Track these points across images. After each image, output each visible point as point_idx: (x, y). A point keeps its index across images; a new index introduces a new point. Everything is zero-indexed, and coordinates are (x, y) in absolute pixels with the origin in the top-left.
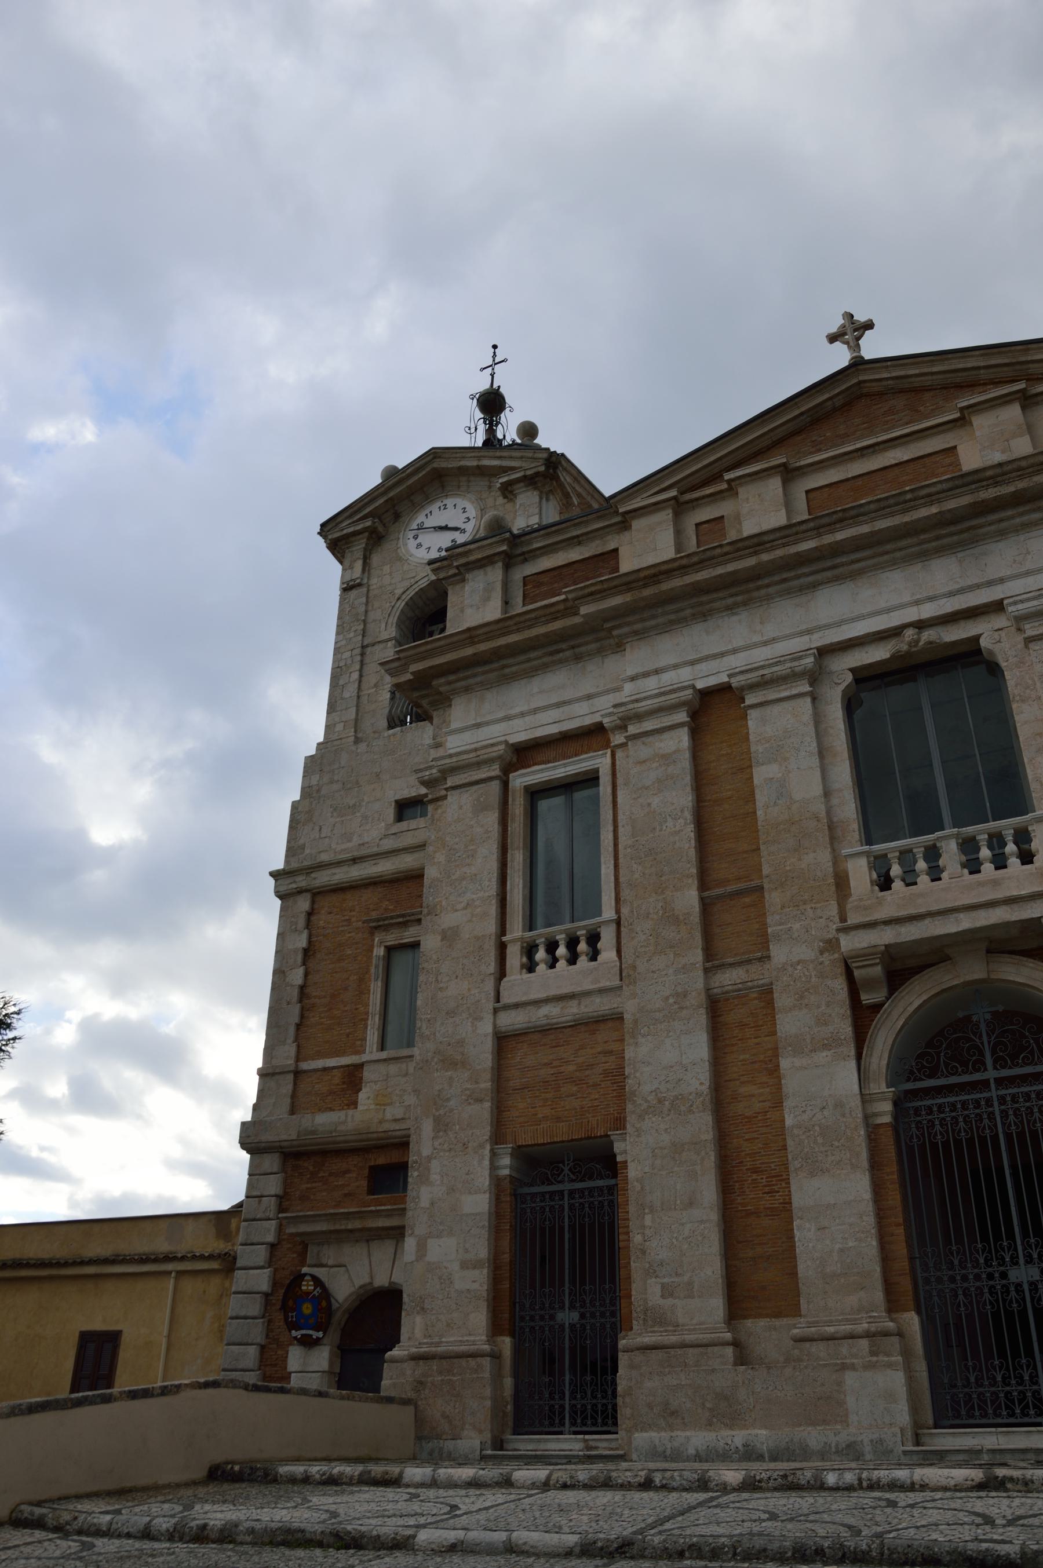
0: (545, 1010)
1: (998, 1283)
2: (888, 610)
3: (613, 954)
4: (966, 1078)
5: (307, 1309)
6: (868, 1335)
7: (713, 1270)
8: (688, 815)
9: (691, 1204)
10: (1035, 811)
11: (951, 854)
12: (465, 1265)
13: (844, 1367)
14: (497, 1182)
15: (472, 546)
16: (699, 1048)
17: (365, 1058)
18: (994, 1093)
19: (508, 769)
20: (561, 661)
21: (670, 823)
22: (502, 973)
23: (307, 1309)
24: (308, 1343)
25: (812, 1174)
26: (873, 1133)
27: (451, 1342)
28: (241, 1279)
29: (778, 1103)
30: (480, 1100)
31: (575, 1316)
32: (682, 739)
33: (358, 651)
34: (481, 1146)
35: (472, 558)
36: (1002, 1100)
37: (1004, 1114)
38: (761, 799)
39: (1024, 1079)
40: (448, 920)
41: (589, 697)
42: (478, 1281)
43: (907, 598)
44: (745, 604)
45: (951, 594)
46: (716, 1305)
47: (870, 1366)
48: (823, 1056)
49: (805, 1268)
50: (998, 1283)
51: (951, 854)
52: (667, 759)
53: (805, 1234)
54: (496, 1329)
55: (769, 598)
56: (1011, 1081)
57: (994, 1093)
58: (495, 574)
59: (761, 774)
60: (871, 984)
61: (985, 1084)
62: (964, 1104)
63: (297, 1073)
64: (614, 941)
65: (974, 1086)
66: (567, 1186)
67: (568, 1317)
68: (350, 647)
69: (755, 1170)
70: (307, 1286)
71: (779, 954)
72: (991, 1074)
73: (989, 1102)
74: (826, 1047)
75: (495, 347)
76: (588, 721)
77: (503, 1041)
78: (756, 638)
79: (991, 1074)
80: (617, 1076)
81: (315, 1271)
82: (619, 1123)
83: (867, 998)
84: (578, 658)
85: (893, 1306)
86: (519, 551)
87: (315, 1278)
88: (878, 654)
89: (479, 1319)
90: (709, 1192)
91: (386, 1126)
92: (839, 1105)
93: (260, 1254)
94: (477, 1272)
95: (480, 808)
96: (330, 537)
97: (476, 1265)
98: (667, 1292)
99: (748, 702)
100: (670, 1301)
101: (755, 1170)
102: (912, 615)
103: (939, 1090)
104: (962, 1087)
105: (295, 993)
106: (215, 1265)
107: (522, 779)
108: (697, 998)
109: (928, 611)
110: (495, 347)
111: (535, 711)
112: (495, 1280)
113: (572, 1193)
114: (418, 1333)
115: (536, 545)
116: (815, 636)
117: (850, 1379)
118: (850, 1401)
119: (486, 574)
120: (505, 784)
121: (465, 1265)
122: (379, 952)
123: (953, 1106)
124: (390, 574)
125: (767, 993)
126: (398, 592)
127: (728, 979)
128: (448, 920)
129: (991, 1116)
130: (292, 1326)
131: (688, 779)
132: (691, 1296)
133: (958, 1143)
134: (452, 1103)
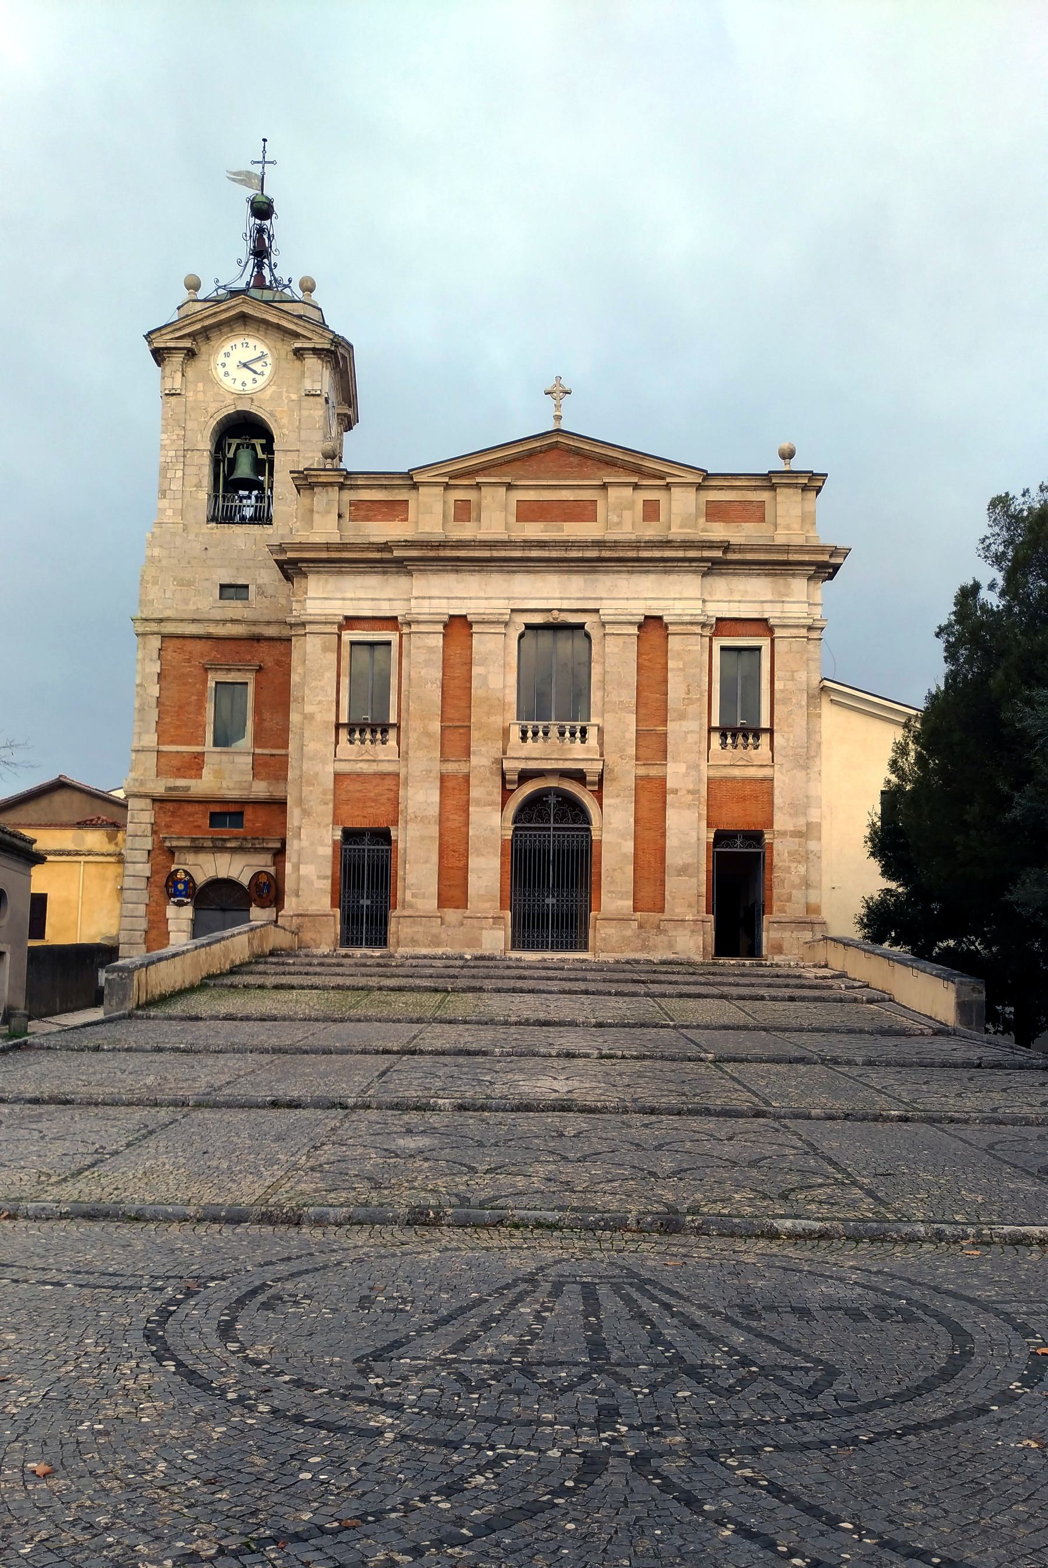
0: (360, 765)
1: (541, 903)
2: (548, 599)
3: (395, 743)
4: (542, 825)
5: (181, 887)
6: (493, 918)
7: (434, 889)
8: (439, 683)
9: (427, 862)
10: (585, 947)
11: (554, 731)
12: (319, 877)
13: (482, 928)
14: (334, 842)
15: (322, 473)
16: (435, 797)
17: (205, 749)
18: (552, 833)
19: (341, 628)
20: (375, 572)
21: (429, 685)
22: (337, 742)
23: (181, 887)
24: (180, 904)
25: (478, 856)
26: (504, 841)
27: (313, 909)
28: (130, 869)
29: (467, 824)
30: (326, 804)
31: (369, 902)
32: (438, 641)
33: (181, 453)
34: (328, 825)
35: (320, 480)
36: (554, 836)
37: (554, 842)
38: (474, 684)
39: (564, 829)
40: (308, 709)
41: (390, 600)
42: (327, 884)
43: (557, 595)
44: (479, 571)
45: (578, 599)
46: (435, 902)
47: (491, 929)
48: (488, 808)
49: (471, 891)
50: (541, 903)
51: (554, 731)
52: (431, 650)
53: (472, 878)
54: (333, 905)
55: (492, 572)
56: (559, 829)
57: (552, 833)
58: (334, 493)
59: (476, 670)
60: (512, 782)
61: (549, 828)
62: (540, 836)
63: (158, 751)
64: (335, 679)
65: (544, 829)
66: (366, 847)
67: (365, 902)
68: (174, 447)
69: (454, 851)
70: (181, 875)
71: (474, 760)
72: (552, 825)
73: (549, 836)
74: (490, 805)
75: (265, 140)
76: (389, 614)
77: (338, 776)
78: (482, 595)
79: (552, 825)
80: (395, 802)
81: (185, 867)
82: (395, 822)
83: (509, 787)
84: (385, 573)
85: (502, 908)
86: (348, 483)
87: (185, 871)
88: (538, 619)
89: (327, 900)
90: (435, 858)
91: (223, 792)
92: (492, 830)
93: (142, 856)
94: (325, 881)
95: (325, 649)
96: (155, 345)
97: (325, 878)
98: (414, 895)
99: (474, 630)
100: (414, 900)
101: (454, 851)
102: (557, 604)
103: (531, 829)
104: (540, 829)
105: (155, 701)
106: (112, 859)
107: (348, 636)
108: (435, 774)
109: (566, 605)
110: (265, 140)
111: (359, 599)
112: (333, 885)
113: (369, 850)
114: (294, 905)
115: (359, 483)
116: (512, 602)
117: (484, 932)
118: (484, 940)
119: (327, 492)
120: (339, 637)
121: (319, 877)
122: (211, 684)
123: (535, 836)
124: (204, 392)
125: (467, 778)
126: (211, 410)
127: (451, 767)
128: (308, 709)
129: (549, 842)
130: (171, 896)
131: (440, 664)
132: (424, 898)
133: (535, 850)
134: (312, 803)
